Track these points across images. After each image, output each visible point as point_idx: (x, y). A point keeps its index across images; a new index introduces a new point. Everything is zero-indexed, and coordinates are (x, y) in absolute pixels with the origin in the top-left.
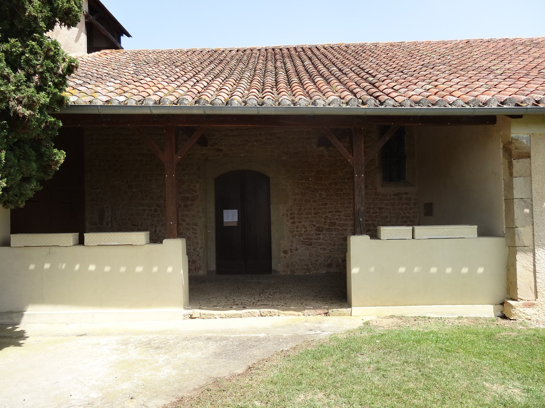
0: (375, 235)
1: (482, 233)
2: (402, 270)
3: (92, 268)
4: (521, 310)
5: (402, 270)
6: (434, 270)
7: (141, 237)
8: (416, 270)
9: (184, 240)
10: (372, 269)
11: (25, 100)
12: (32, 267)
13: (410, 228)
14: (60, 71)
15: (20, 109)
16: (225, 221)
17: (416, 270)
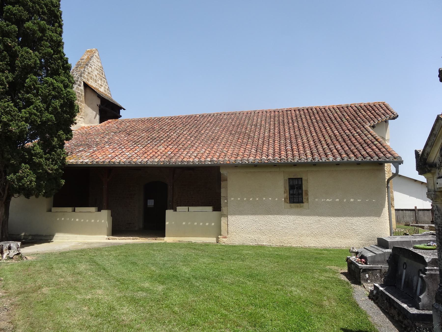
0: (175, 210)
1: (214, 210)
2: (184, 223)
3: (77, 220)
4: (222, 239)
5: (184, 223)
6: (196, 224)
7: (93, 209)
8: (189, 223)
9: (110, 211)
10: (173, 223)
11: (51, 169)
12: (58, 219)
13: (187, 207)
14: (61, 159)
15: (49, 171)
16: (148, 204)
17: (189, 223)
